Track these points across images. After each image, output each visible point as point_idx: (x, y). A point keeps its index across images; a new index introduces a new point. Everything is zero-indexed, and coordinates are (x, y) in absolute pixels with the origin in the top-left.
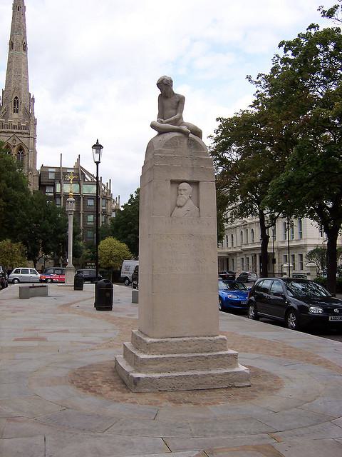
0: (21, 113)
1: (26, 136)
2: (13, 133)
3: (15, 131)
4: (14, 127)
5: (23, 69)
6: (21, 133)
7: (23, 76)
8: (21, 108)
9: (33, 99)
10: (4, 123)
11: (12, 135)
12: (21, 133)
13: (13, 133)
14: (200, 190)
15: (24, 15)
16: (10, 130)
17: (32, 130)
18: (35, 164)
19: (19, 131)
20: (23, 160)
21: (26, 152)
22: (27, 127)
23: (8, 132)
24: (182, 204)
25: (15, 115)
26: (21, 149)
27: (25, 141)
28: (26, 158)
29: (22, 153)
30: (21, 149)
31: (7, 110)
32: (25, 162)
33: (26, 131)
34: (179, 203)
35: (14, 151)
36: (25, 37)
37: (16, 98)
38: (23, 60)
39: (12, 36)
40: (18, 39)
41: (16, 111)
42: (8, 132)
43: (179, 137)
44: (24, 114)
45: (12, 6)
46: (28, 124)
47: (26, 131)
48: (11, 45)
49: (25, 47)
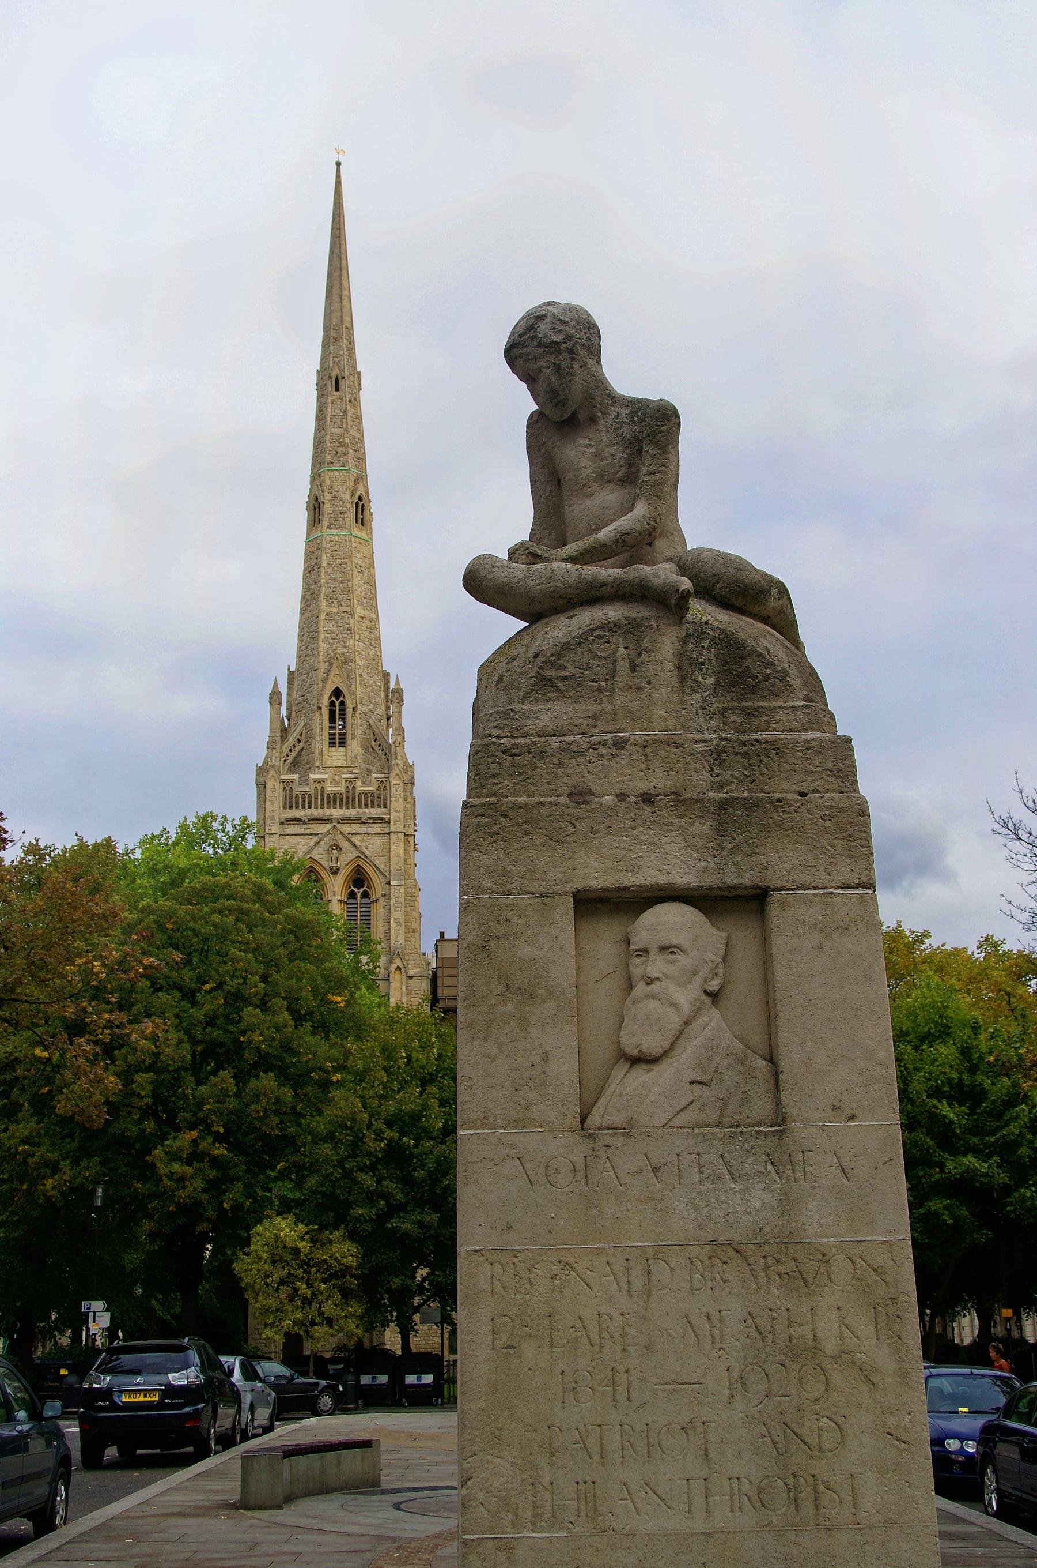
0: (355, 746)
1: (377, 828)
2: (326, 820)
3: (337, 813)
4: (333, 800)
5: (359, 588)
6: (358, 820)
7: (359, 611)
8: (356, 727)
9: (399, 692)
10: (298, 789)
11: (324, 828)
12: (358, 820)
13: (326, 820)
14: (779, 942)
15: (355, 401)
16: (316, 812)
17: (397, 803)
18: (412, 931)
19: (352, 812)
20: (367, 918)
21: (378, 890)
22: (378, 798)
23: (313, 820)
24: (652, 1044)
25: (337, 756)
26: (359, 879)
27: (372, 846)
28: (378, 911)
29: (365, 895)
30: (359, 879)
31: (305, 739)
32: (378, 931)
33: (374, 812)
34: (633, 1041)
35: (336, 889)
36: (361, 478)
37: (337, 693)
38: (358, 559)
39: (316, 477)
40: (337, 478)
41: (338, 740)
42: (313, 820)
43: (633, 628)
44: (367, 748)
45: (314, 379)
46: (383, 786)
47: (374, 812)
48: (315, 507)
49: (361, 509)
